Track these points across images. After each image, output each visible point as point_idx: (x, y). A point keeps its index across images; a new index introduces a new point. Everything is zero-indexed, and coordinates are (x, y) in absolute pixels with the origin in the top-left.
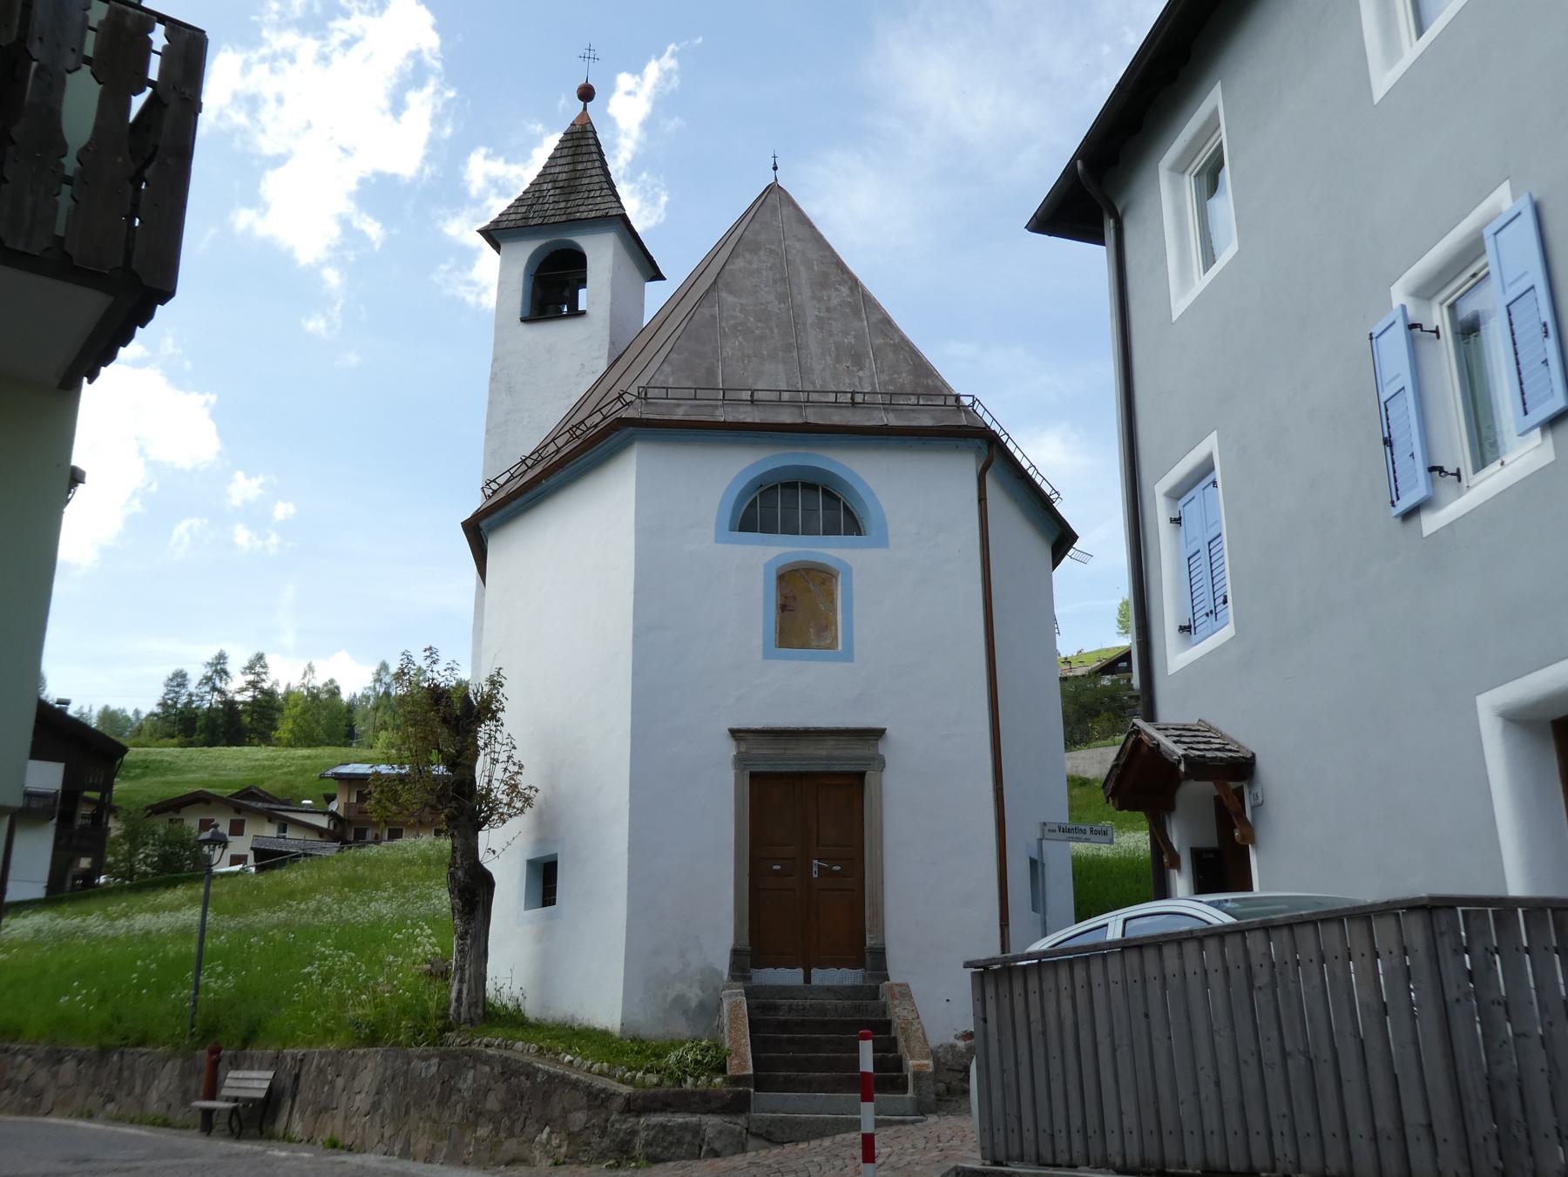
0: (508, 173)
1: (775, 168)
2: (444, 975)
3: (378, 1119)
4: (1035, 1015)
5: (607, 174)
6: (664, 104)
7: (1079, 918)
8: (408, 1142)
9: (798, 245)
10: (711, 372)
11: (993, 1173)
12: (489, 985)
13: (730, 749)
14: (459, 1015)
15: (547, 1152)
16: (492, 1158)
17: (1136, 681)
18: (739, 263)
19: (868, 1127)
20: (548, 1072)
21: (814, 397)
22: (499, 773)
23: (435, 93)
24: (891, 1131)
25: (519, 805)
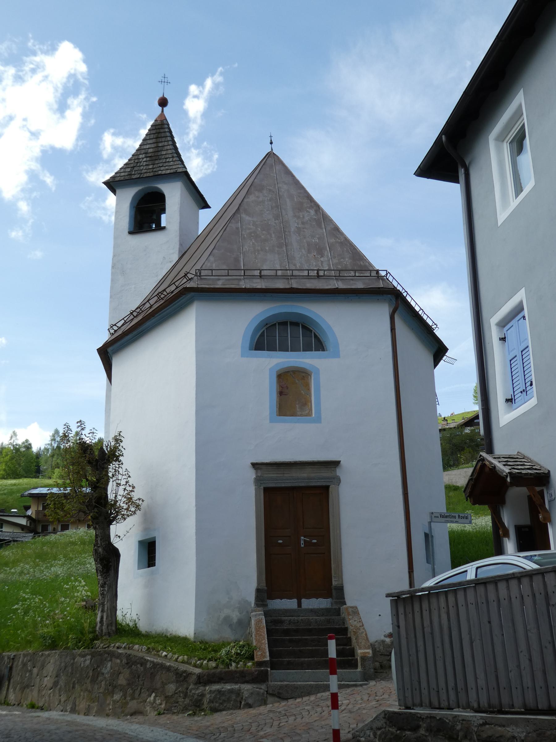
0: (120, 146)
1: (271, 143)
2: (93, 608)
3: (57, 692)
4: (427, 623)
5: (176, 148)
6: (214, 103)
7: (454, 566)
8: (74, 704)
9: (285, 187)
10: (237, 260)
11: (405, 713)
12: (119, 613)
13: (252, 474)
14: (102, 630)
15: (154, 707)
16: (123, 712)
17: (482, 432)
18: (252, 198)
19: (334, 689)
20: (153, 662)
21: (295, 273)
22: (121, 492)
23: (85, 99)
24: (349, 690)
25: (133, 509)
